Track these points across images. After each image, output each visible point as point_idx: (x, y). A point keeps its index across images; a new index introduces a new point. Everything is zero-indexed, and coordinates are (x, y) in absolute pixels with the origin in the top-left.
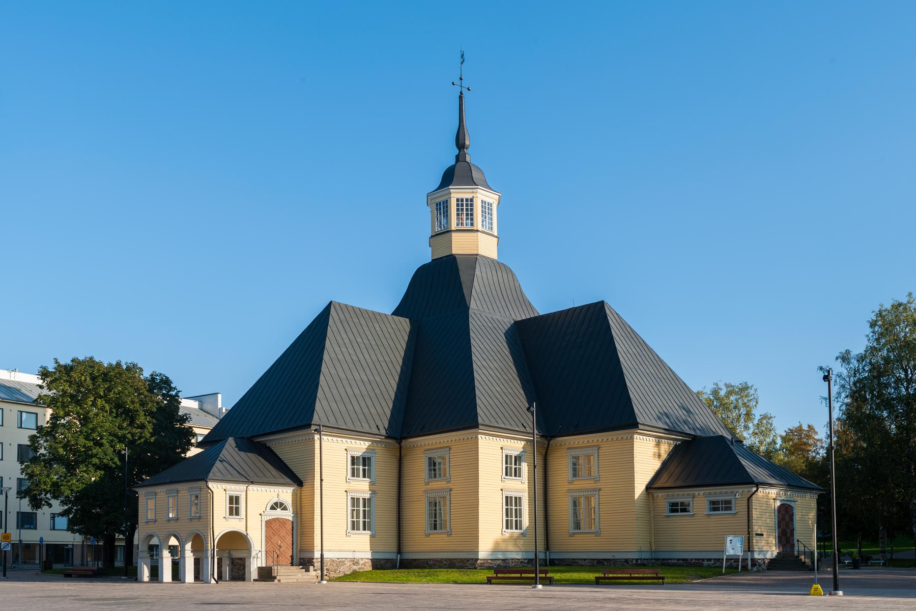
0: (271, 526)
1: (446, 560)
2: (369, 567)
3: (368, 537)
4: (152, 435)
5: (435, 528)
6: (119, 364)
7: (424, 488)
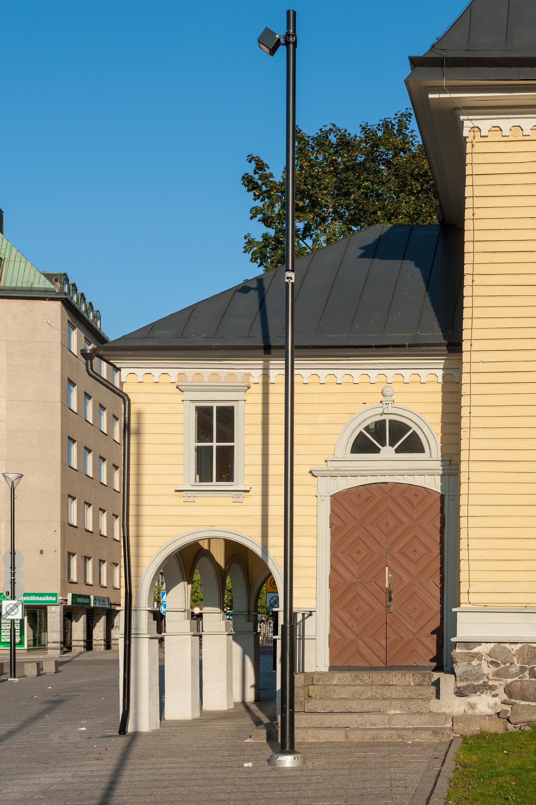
5: (311, 472)
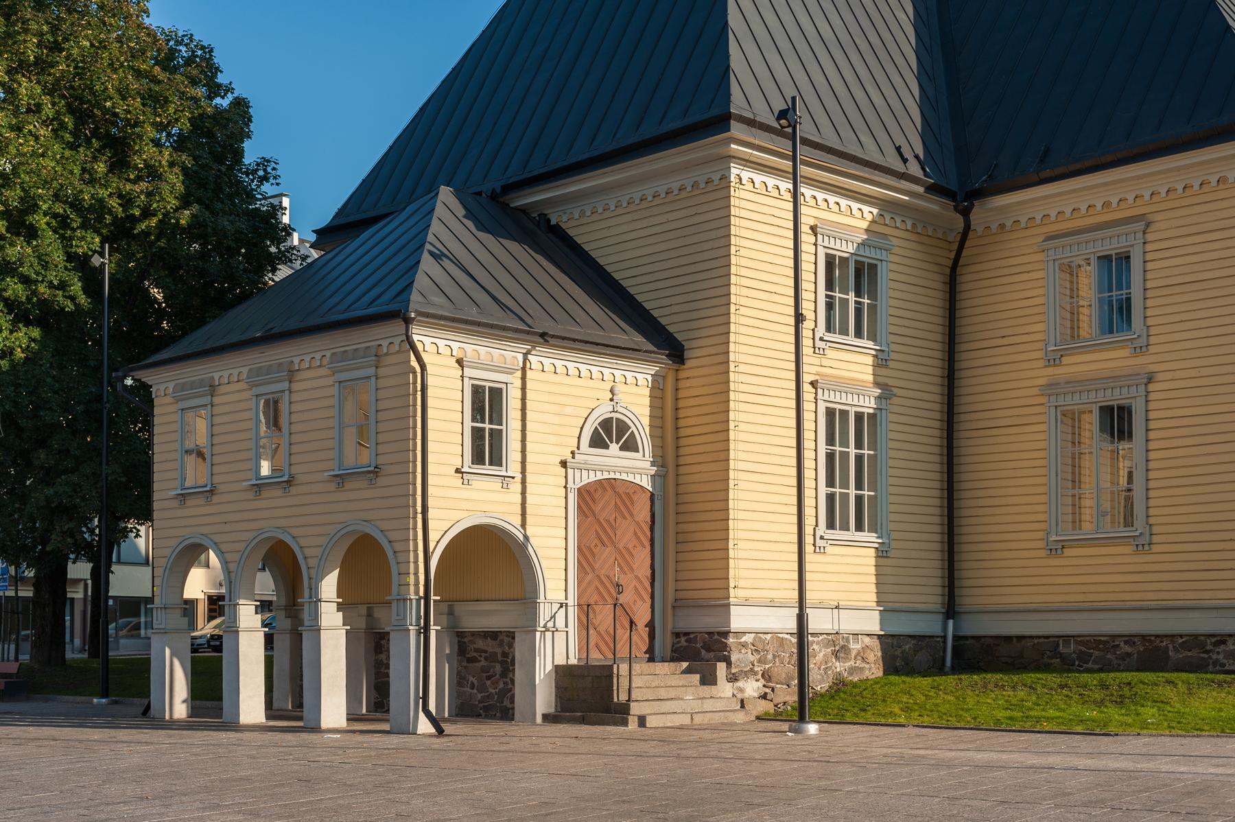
0: (595, 502)
1: (1130, 639)
2: (873, 670)
3: (867, 559)
4: (185, 201)
7: (1044, 375)
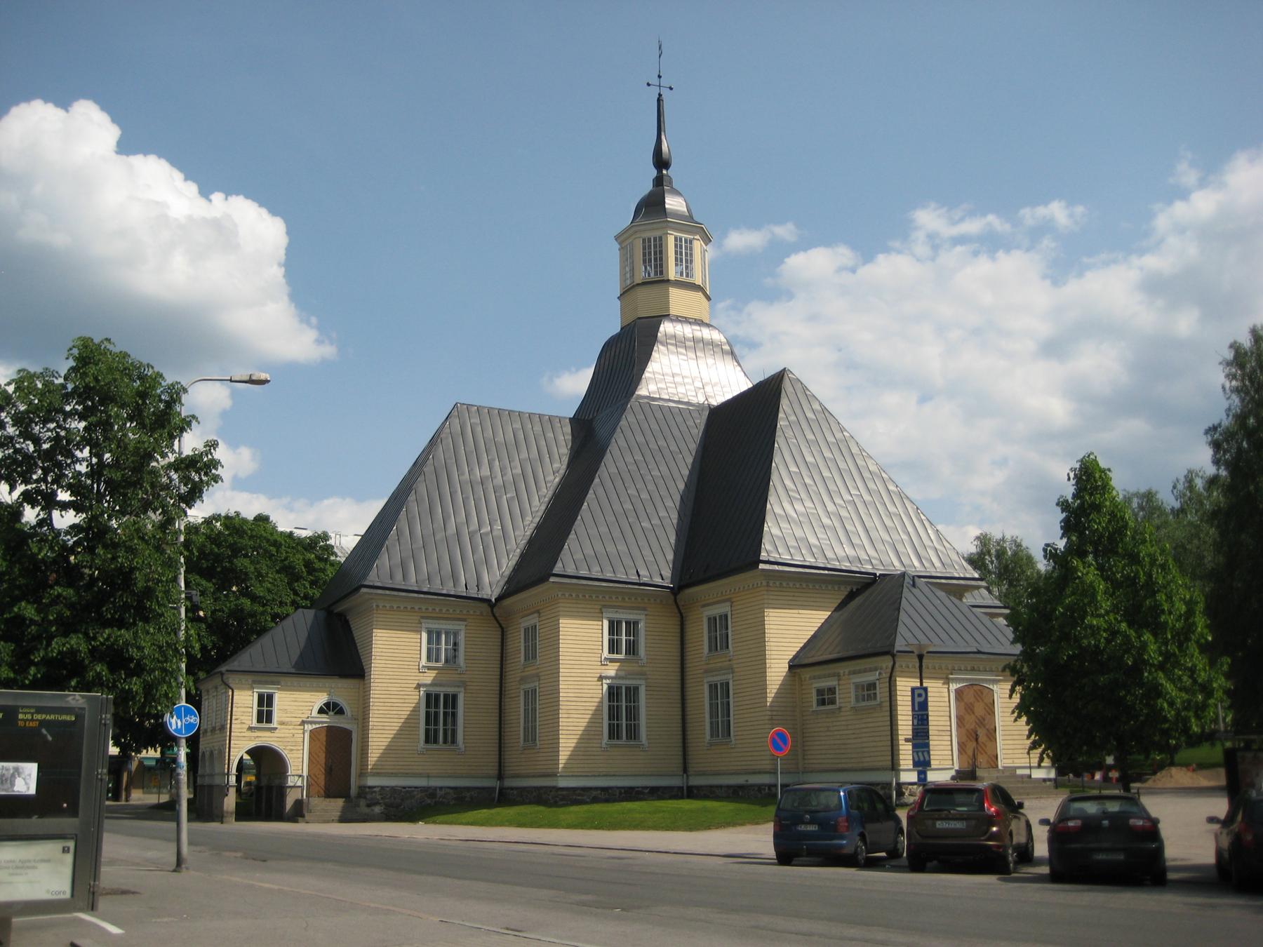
6: (1064, 505)
